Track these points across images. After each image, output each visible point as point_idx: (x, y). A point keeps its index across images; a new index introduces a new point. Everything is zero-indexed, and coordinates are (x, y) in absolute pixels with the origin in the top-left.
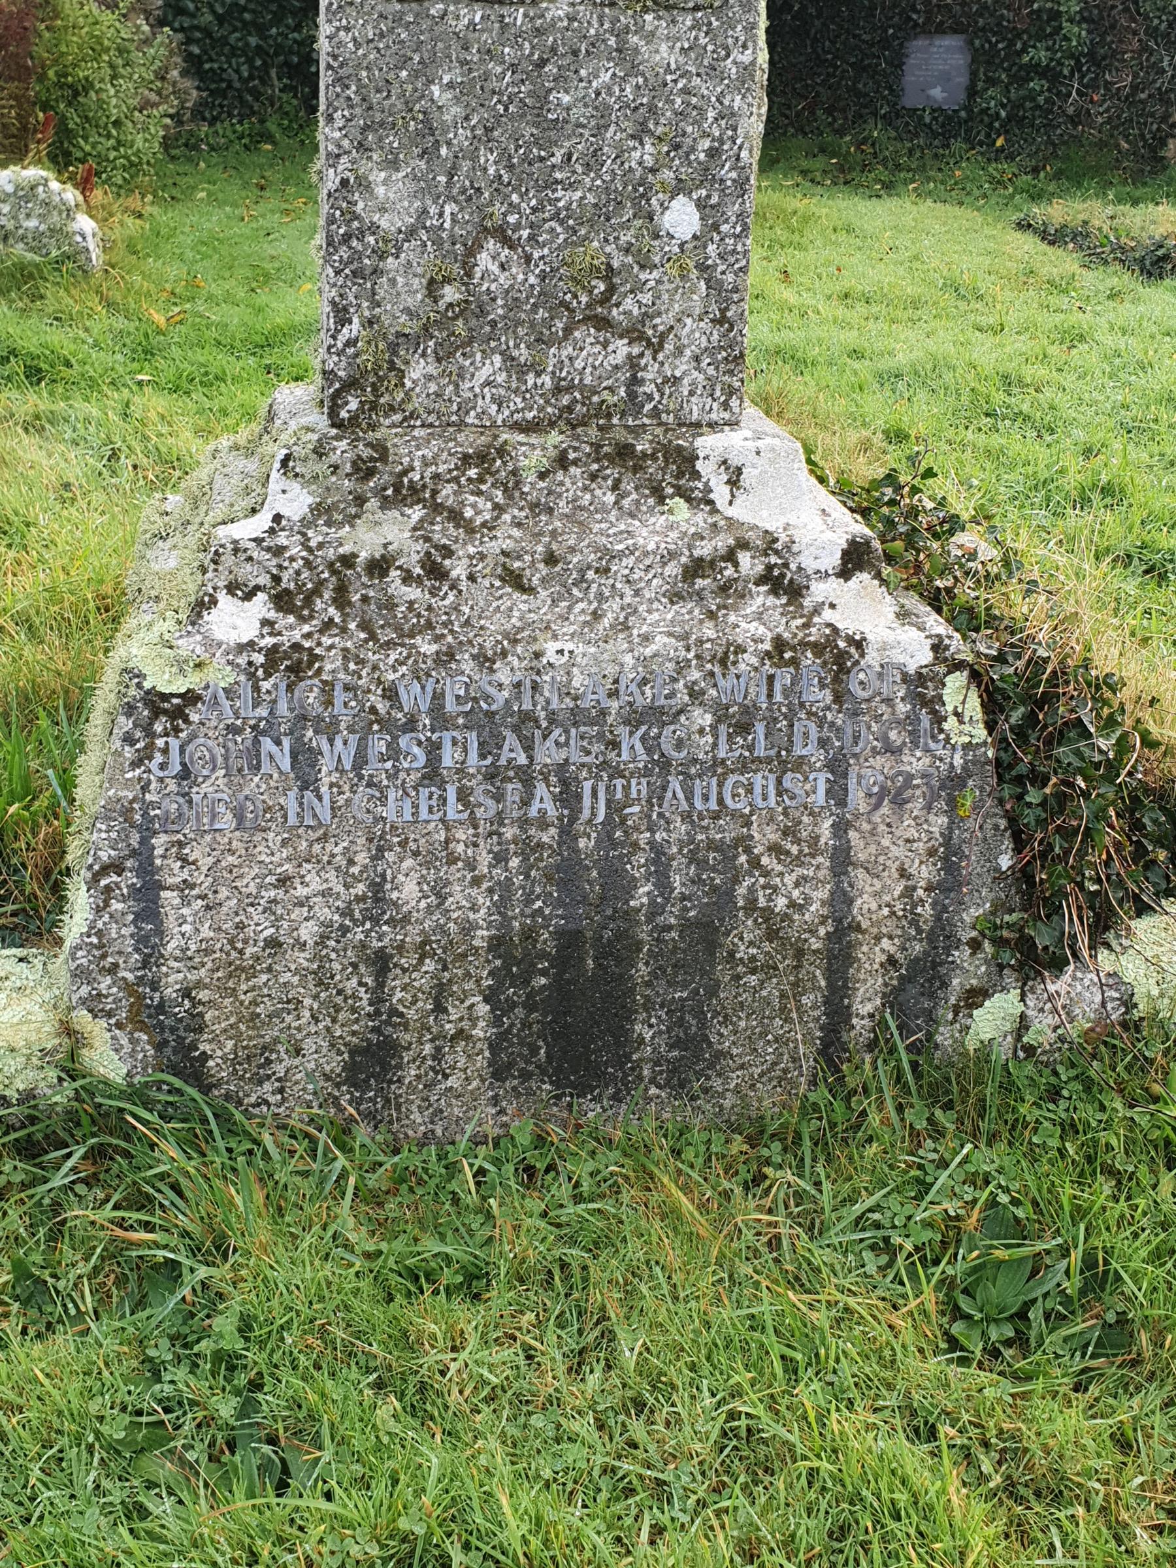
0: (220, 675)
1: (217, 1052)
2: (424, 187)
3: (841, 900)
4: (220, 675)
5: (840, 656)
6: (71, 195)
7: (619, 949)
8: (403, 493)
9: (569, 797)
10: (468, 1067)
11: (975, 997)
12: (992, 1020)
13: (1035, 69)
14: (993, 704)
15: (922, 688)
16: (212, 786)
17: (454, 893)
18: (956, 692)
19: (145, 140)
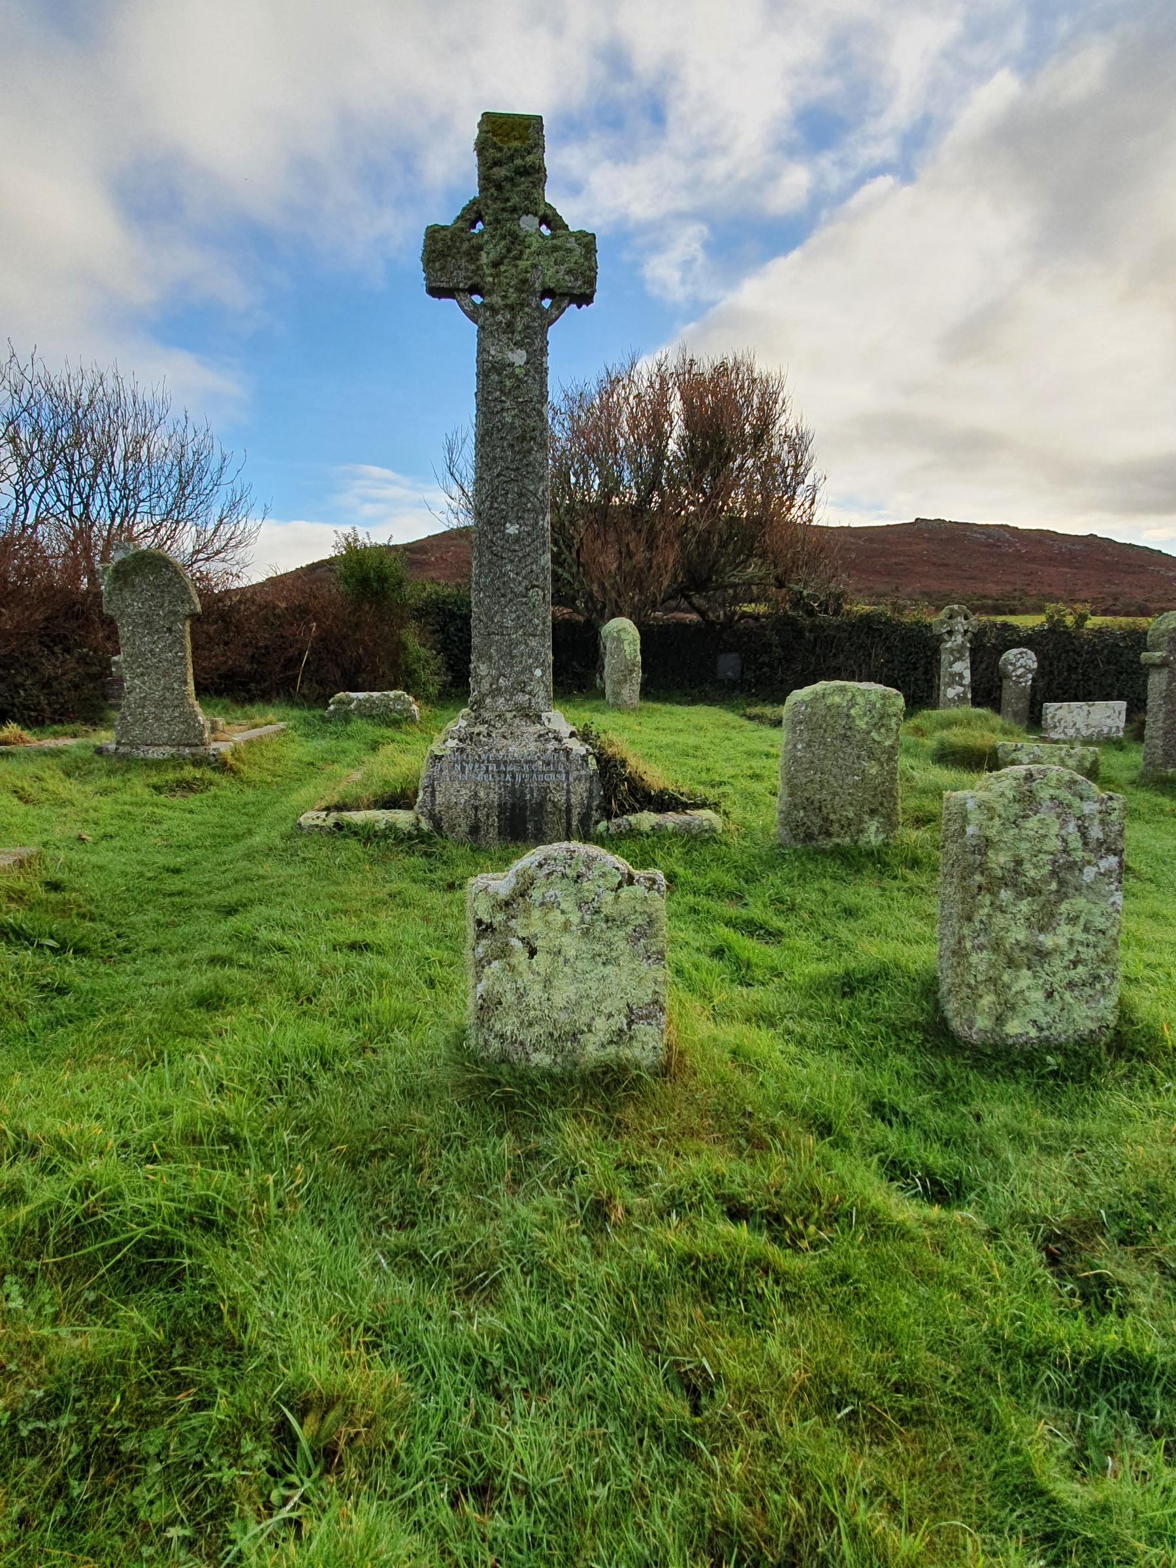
0: (448, 752)
1: (445, 826)
2: (489, 667)
3: (568, 800)
4: (448, 752)
5: (568, 752)
6: (411, 699)
7: (523, 808)
8: (484, 722)
9: (513, 777)
10: (493, 833)
11: (597, 822)
12: (602, 826)
13: (764, 664)
14: (598, 761)
15: (584, 758)
16: (446, 772)
17: (491, 795)
18: (592, 761)
19: (433, 690)
